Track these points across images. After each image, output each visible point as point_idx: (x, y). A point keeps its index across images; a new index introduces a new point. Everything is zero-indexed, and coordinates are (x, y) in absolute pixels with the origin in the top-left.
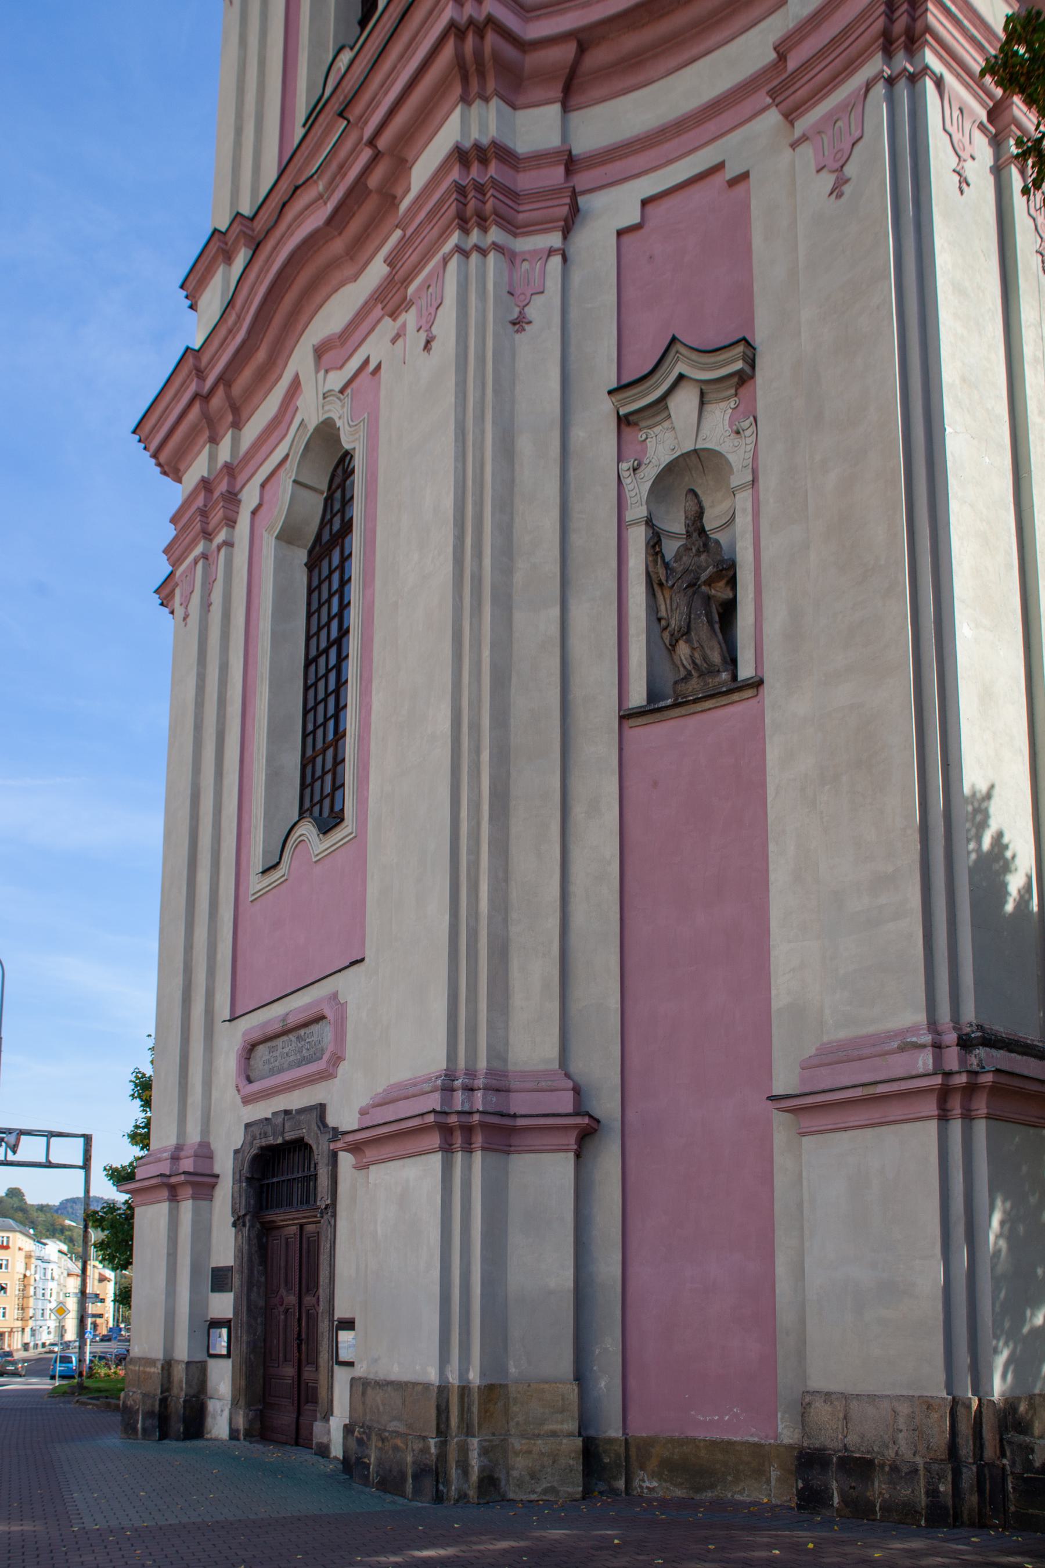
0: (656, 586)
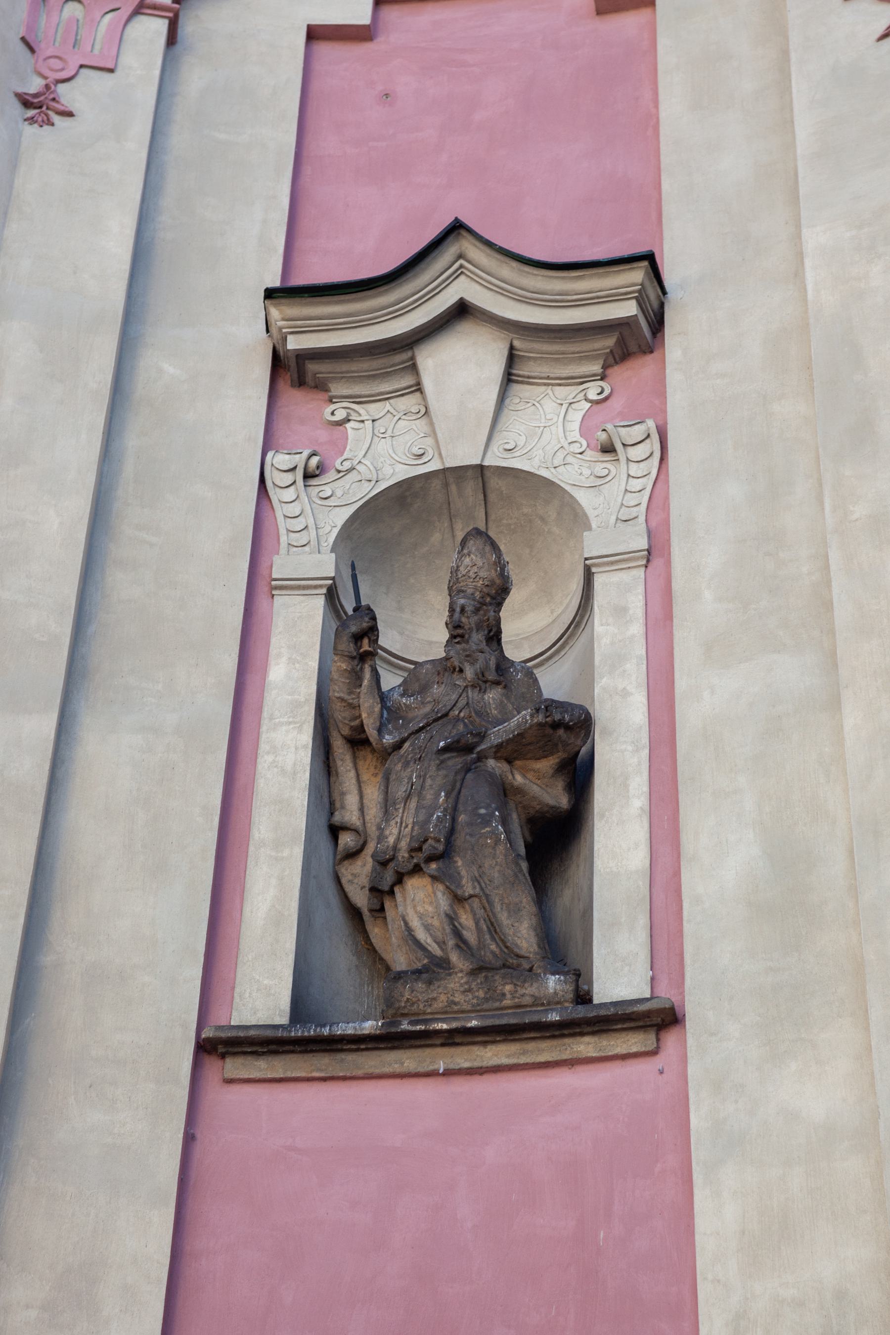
0: (339, 746)
